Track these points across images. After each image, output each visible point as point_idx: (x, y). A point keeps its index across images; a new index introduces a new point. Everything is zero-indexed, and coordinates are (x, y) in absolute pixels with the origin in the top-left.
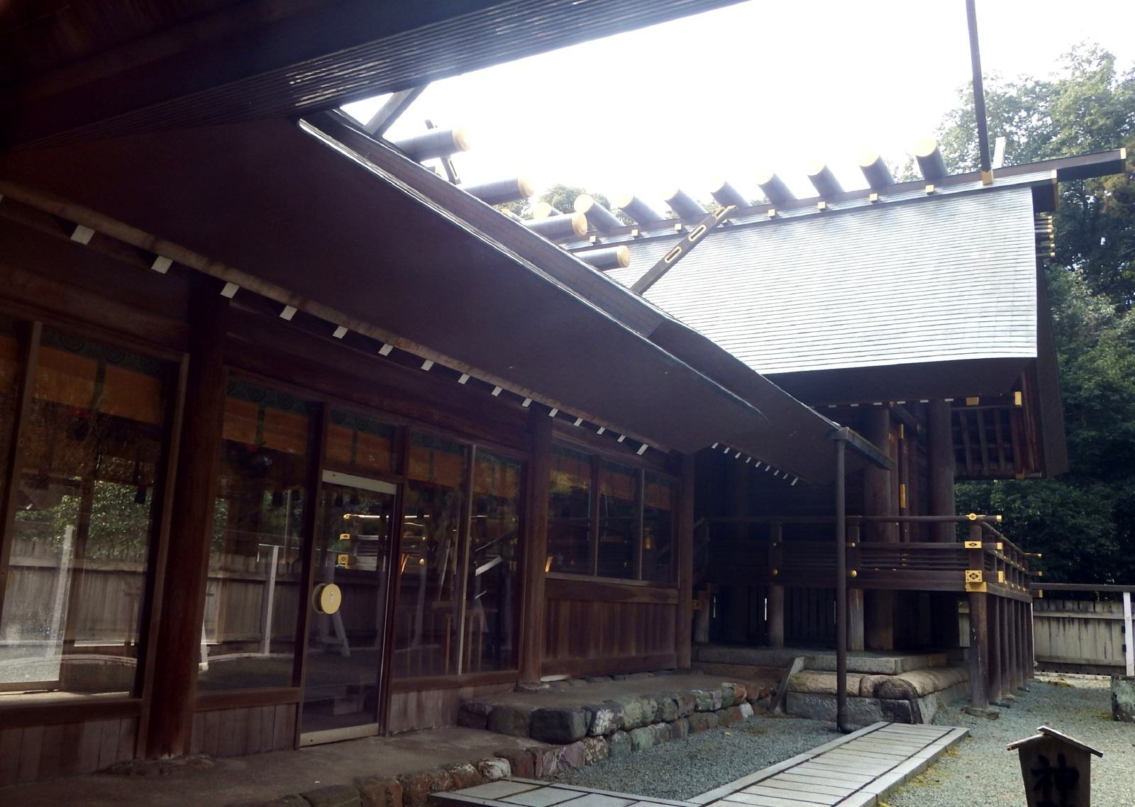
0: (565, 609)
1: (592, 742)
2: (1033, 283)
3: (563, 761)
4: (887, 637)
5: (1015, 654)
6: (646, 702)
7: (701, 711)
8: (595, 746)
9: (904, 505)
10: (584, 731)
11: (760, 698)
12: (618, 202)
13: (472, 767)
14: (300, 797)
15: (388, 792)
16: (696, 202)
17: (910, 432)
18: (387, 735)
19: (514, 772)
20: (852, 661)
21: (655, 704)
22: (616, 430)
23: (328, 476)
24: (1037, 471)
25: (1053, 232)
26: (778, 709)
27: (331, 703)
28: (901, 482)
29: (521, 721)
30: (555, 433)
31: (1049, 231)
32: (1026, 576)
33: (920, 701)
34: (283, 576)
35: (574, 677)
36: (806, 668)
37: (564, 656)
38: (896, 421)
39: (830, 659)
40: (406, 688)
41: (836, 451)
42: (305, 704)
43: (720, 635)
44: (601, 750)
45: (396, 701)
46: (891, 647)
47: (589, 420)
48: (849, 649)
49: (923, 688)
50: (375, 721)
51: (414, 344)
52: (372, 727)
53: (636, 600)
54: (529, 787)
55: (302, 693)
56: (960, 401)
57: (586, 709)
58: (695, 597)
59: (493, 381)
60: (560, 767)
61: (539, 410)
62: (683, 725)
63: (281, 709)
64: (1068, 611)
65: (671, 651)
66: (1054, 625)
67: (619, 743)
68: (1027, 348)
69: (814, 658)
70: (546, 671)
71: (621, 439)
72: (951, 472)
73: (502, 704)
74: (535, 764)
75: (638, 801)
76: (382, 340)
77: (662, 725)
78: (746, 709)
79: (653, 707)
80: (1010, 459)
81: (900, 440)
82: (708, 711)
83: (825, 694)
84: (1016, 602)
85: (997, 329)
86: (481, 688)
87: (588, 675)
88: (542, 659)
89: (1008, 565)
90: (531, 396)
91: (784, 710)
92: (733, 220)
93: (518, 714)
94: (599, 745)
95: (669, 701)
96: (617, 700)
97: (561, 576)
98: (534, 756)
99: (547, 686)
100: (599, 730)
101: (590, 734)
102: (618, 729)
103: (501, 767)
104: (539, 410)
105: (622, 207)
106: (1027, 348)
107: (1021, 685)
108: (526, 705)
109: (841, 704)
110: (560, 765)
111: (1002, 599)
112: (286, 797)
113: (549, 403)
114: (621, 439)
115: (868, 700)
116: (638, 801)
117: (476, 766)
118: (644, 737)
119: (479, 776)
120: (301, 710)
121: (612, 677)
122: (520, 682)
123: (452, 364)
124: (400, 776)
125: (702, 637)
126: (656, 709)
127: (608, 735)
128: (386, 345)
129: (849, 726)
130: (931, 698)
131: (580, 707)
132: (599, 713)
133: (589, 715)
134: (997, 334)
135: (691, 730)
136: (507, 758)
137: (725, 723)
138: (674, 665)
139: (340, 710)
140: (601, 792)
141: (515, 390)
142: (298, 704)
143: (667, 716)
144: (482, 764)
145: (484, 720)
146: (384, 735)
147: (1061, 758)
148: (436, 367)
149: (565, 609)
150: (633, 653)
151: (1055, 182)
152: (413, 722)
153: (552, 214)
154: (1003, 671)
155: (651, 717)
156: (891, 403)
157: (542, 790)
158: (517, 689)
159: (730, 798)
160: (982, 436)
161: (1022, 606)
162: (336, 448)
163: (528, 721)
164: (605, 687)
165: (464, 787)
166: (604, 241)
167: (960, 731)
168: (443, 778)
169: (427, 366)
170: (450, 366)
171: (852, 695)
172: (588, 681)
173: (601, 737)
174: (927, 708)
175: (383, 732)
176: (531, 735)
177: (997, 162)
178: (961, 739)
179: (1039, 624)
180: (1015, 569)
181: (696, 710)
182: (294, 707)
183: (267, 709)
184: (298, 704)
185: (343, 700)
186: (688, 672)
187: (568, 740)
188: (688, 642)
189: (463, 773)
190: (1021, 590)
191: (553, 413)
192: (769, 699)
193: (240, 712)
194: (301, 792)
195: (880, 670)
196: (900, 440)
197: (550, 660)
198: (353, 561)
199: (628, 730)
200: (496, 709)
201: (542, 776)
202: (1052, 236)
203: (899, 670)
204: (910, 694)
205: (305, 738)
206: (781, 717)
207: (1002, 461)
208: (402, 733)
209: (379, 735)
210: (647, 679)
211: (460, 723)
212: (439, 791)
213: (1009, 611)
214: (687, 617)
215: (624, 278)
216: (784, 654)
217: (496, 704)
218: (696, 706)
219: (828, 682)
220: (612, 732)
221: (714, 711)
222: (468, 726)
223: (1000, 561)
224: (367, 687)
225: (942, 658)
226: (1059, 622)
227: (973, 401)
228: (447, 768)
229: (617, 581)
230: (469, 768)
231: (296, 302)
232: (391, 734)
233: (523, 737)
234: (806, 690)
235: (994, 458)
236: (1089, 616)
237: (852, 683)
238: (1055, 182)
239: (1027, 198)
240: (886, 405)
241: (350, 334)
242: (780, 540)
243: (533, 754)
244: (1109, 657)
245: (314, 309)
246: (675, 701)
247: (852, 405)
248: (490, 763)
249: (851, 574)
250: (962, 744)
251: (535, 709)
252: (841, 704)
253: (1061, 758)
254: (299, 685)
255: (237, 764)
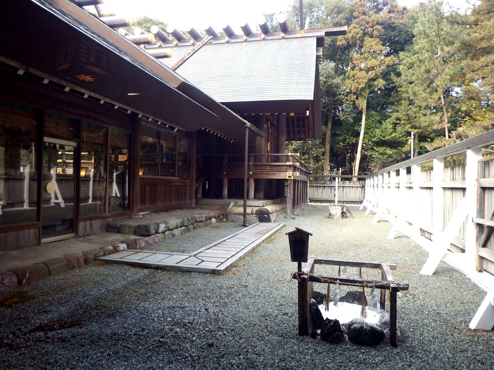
0: (148, 188)
1: (158, 235)
2: (314, 72)
3: (147, 242)
4: (262, 194)
5: (301, 198)
6: (178, 220)
7: (198, 222)
8: (159, 237)
9: (269, 149)
10: (155, 232)
11: (219, 216)
12: (170, 30)
13: (112, 247)
14: (42, 264)
15: (78, 258)
16: (200, 34)
17: (272, 124)
18: (78, 237)
19: (128, 248)
20: (249, 203)
21: (181, 221)
22: (165, 123)
23: (46, 139)
24: (312, 138)
25: (322, 55)
26: (225, 220)
27: (55, 226)
28: (268, 142)
29: (131, 229)
30: (143, 123)
31: (321, 54)
32: (307, 173)
33: (271, 215)
34: (32, 176)
35: (152, 212)
36: (235, 206)
37: (147, 205)
38: (267, 120)
39: (241, 202)
40: (85, 220)
41: (245, 131)
42: (42, 227)
43: (206, 195)
44: (161, 238)
45: (81, 225)
46: (263, 197)
47: (154, 119)
48: (248, 198)
49: (272, 211)
50: (73, 232)
51: (79, 87)
52: (72, 235)
53: (175, 184)
54: (134, 253)
55: (40, 224)
56: (288, 114)
57: (156, 224)
58: (196, 182)
59: (114, 103)
60: (146, 244)
61: (134, 115)
62: (191, 227)
63: (32, 231)
64: (319, 184)
65: (188, 201)
66: (315, 188)
67: (168, 235)
68: (310, 96)
69: (237, 202)
70: (141, 210)
71: (167, 126)
72: (284, 138)
73: (124, 223)
74: (136, 244)
75: (173, 255)
76: (65, 85)
77: (184, 228)
78: (214, 220)
79: (180, 222)
80: (305, 134)
81: (268, 127)
82: (200, 222)
83: (240, 214)
84: (303, 181)
85: (301, 89)
86: (116, 218)
87: (157, 211)
88: (139, 207)
89: (301, 170)
90: (130, 109)
91: (227, 220)
92: (212, 41)
93: (130, 227)
94: (160, 236)
95: (186, 219)
96: (167, 220)
97: (146, 176)
98: (136, 242)
99: (141, 216)
100: (160, 231)
101: (157, 232)
102: (168, 230)
103: (123, 246)
104: (134, 115)
105: (188, 31)
106: (310, 96)
107: (303, 208)
108: (133, 223)
109: (245, 217)
110: (146, 244)
111: (298, 181)
112: (35, 264)
113: (138, 112)
114: (167, 126)
115: (254, 216)
116: (173, 255)
117: (113, 246)
118: (177, 232)
119: (115, 250)
120: (41, 230)
121: (166, 211)
122: (131, 215)
123: (97, 96)
124: (83, 252)
125: (200, 196)
126: (181, 222)
127: (163, 232)
128: (67, 88)
129: (247, 225)
130: (275, 214)
131: (153, 223)
132: (160, 225)
133: (156, 226)
134: (301, 91)
135: (194, 228)
136: (125, 243)
137: (206, 225)
138: (189, 206)
139: (59, 228)
140: (163, 253)
141: (124, 107)
142: (39, 228)
143: (185, 224)
144: (116, 246)
145: (118, 230)
146: (77, 237)
147: (300, 237)
148: (89, 96)
149: (148, 188)
150: (174, 203)
151: (324, 36)
152: (88, 231)
153: (142, 33)
154: (298, 204)
155: (180, 225)
156: (266, 114)
157: (138, 254)
158: (130, 218)
159: (205, 251)
160: (296, 126)
161: (305, 183)
162: (50, 126)
163: (134, 229)
164: (164, 215)
165: (109, 254)
166: (163, 45)
167: (282, 224)
168: (100, 252)
169: (86, 96)
170: (95, 96)
171: (249, 214)
172: (157, 213)
173: (161, 233)
174: (273, 217)
175: (77, 236)
176: (135, 234)
177: (306, 27)
178: (283, 227)
179: (310, 188)
180: (303, 171)
181: (196, 221)
182: (38, 229)
183: (26, 232)
184: (39, 228)
185: (60, 225)
186: (194, 208)
187: (149, 235)
188: (194, 198)
189: (108, 249)
190: (305, 178)
191: (140, 116)
192: (221, 216)
193: (14, 233)
194: (42, 261)
195: (258, 205)
196: (268, 127)
197: (142, 207)
198: (64, 171)
199: (171, 230)
200: (122, 226)
201: (139, 248)
202: (322, 56)
203: (265, 205)
204: (268, 213)
205: (43, 240)
206: (225, 222)
207: (302, 135)
208: (84, 236)
209: (75, 237)
210: (179, 212)
211: (108, 231)
212: (99, 257)
213: (300, 185)
214: (194, 189)
215: (168, 63)
216: (227, 201)
217: (122, 223)
218: (196, 220)
219: (241, 210)
220: (165, 231)
221: (202, 222)
222: (111, 232)
223: (298, 168)
224: (70, 220)
225: (279, 200)
226: (316, 187)
227: (292, 114)
228: (102, 248)
229: (168, 178)
230: (111, 248)
231: (24, 68)
232: (80, 237)
233: (132, 235)
234: (234, 213)
235: (299, 133)
236: (325, 185)
237: (249, 210)
238: (324, 36)
239: (314, 41)
240: (264, 114)
241: (50, 82)
242: (227, 162)
243: (135, 241)
244: (330, 198)
245: (33, 71)
246: (188, 219)
247: (253, 114)
248: (119, 245)
249: (250, 174)
250: (284, 227)
251: (137, 224)
252: (245, 217)
253: (300, 237)
254: (39, 221)
255: (14, 253)
